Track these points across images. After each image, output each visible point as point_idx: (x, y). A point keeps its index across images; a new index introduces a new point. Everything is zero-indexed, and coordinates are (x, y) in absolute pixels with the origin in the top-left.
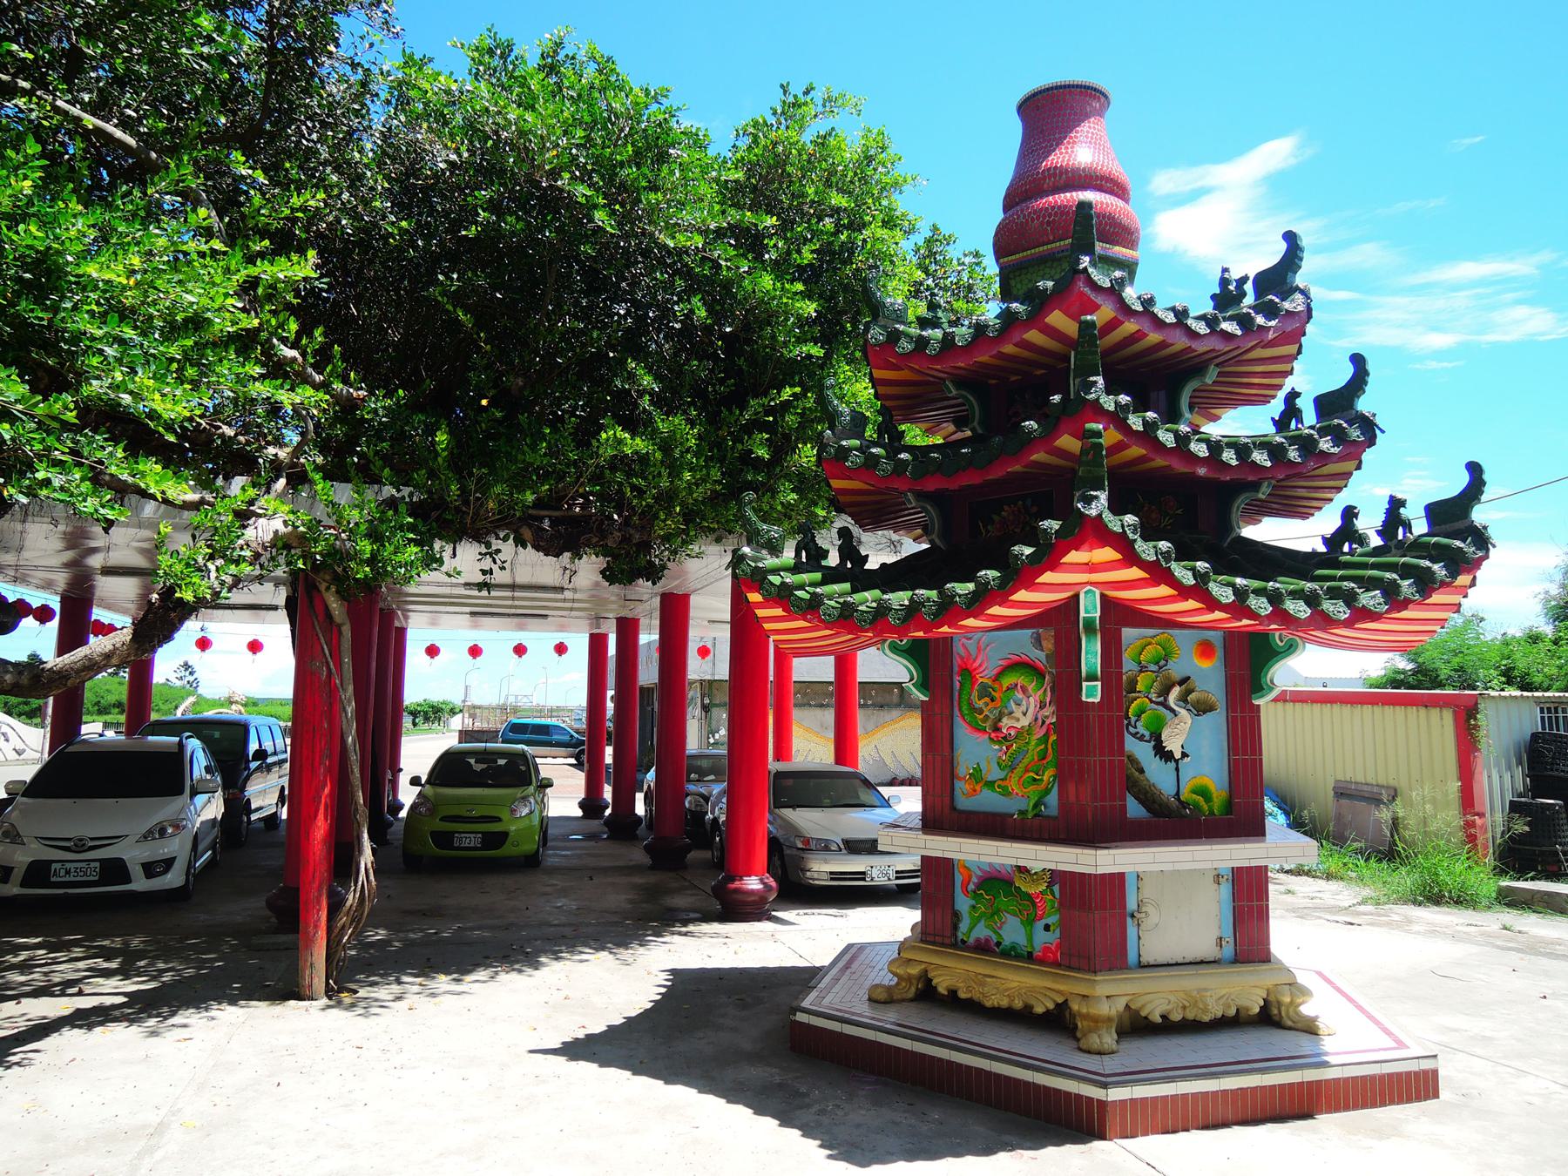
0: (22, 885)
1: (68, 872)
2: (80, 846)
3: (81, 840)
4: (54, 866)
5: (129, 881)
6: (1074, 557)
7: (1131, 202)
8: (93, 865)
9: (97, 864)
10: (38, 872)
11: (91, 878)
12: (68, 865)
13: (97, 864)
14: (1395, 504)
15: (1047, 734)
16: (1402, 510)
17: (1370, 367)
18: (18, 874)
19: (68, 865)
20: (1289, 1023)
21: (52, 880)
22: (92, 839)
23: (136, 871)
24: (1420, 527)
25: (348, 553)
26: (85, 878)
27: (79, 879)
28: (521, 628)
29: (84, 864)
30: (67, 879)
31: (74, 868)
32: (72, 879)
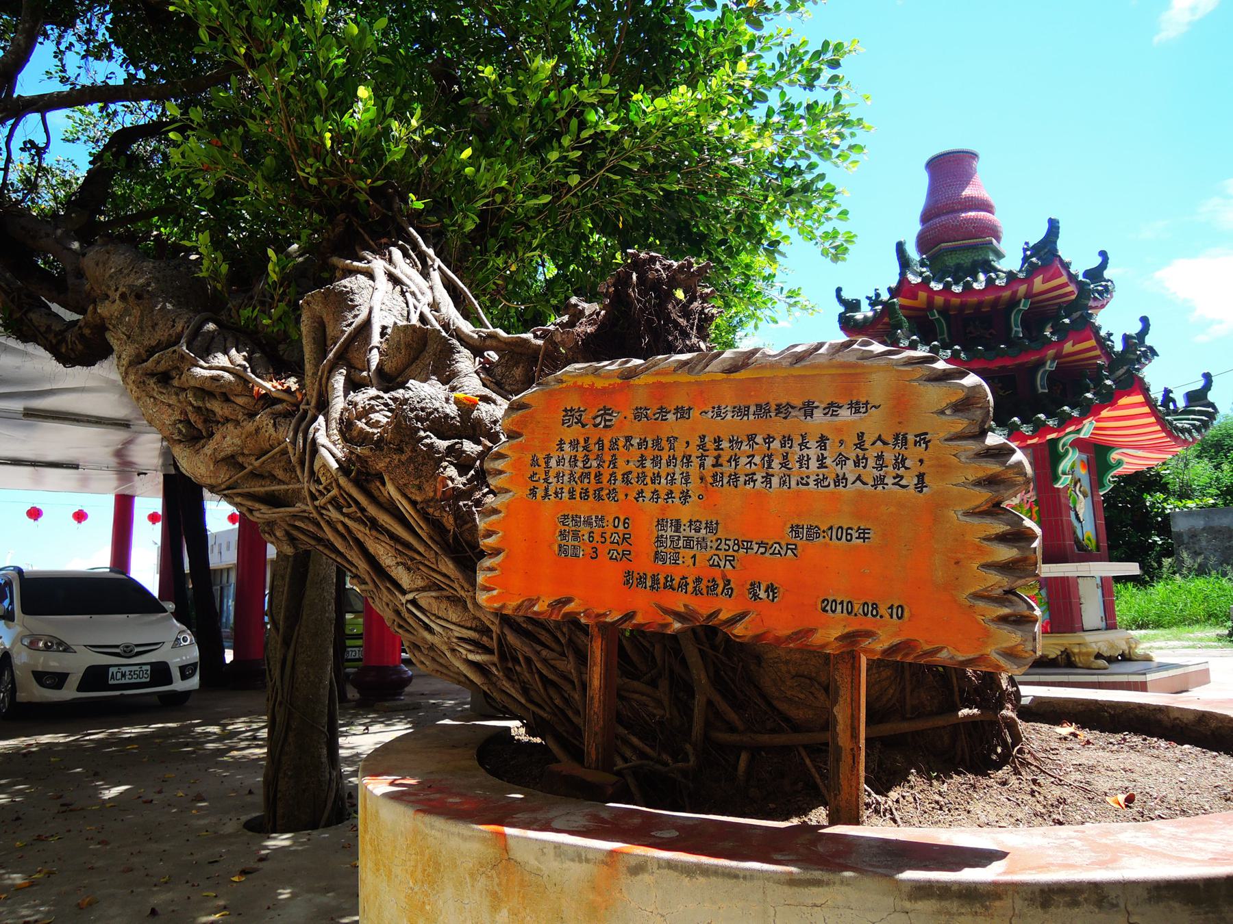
0: (79, 689)
1: (123, 675)
2: (128, 651)
3: (127, 647)
4: (111, 670)
5: (170, 682)
6: (1124, 401)
7: (996, 213)
8: (144, 668)
9: (148, 667)
10: (95, 677)
11: (144, 680)
12: (123, 669)
13: (148, 667)
14: (1167, 392)
15: (1031, 509)
16: (1171, 395)
17: (1151, 322)
18: (74, 681)
19: (123, 669)
20: (1080, 665)
21: (110, 682)
22: (137, 646)
23: (176, 673)
24: (1181, 404)
25: (455, 374)
26: (138, 680)
27: (133, 681)
28: (37, 483)
29: (137, 668)
30: (123, 681)
31: (127, 671)
32: (127, 681)
